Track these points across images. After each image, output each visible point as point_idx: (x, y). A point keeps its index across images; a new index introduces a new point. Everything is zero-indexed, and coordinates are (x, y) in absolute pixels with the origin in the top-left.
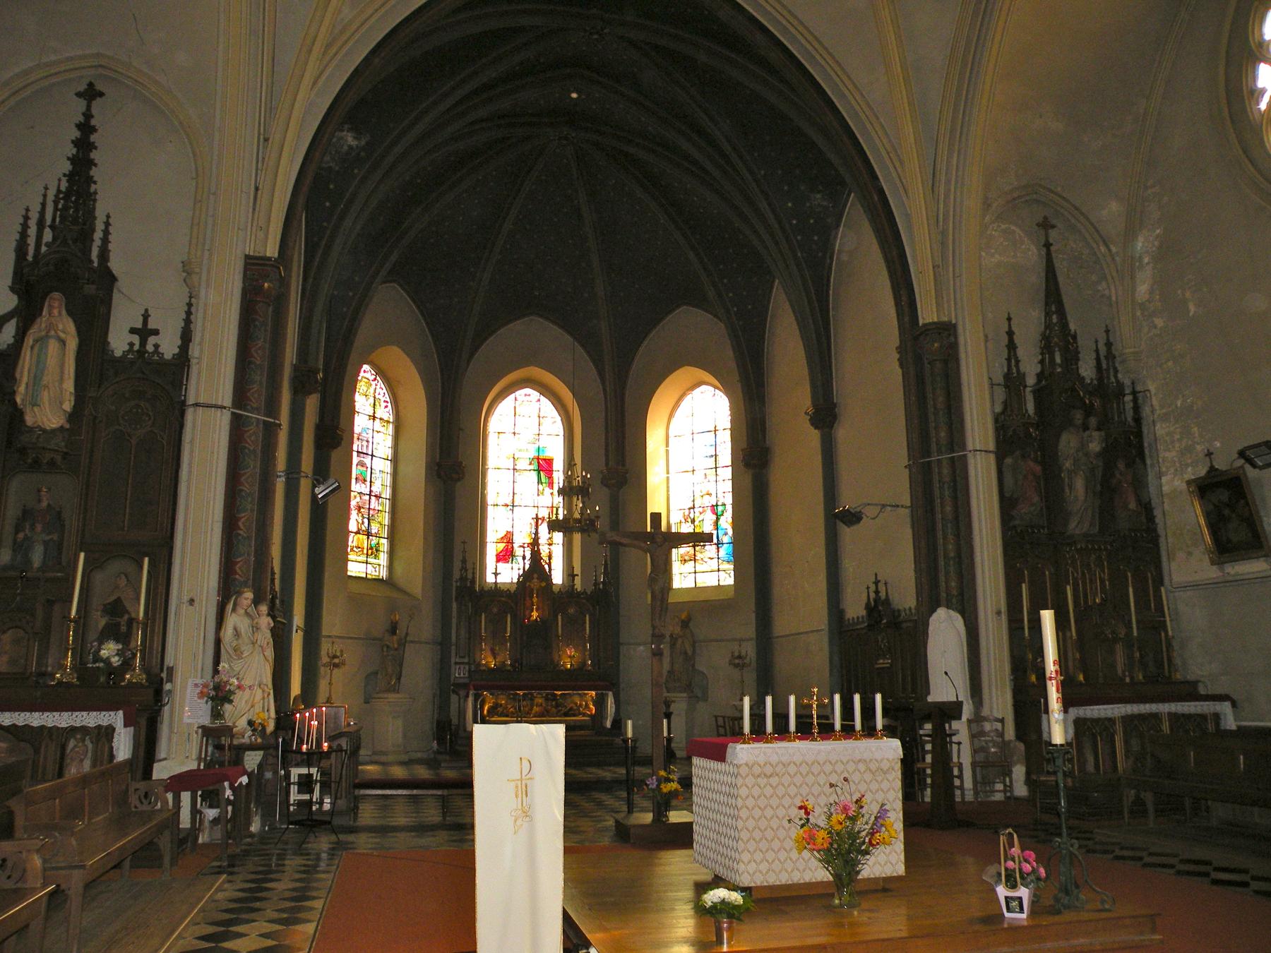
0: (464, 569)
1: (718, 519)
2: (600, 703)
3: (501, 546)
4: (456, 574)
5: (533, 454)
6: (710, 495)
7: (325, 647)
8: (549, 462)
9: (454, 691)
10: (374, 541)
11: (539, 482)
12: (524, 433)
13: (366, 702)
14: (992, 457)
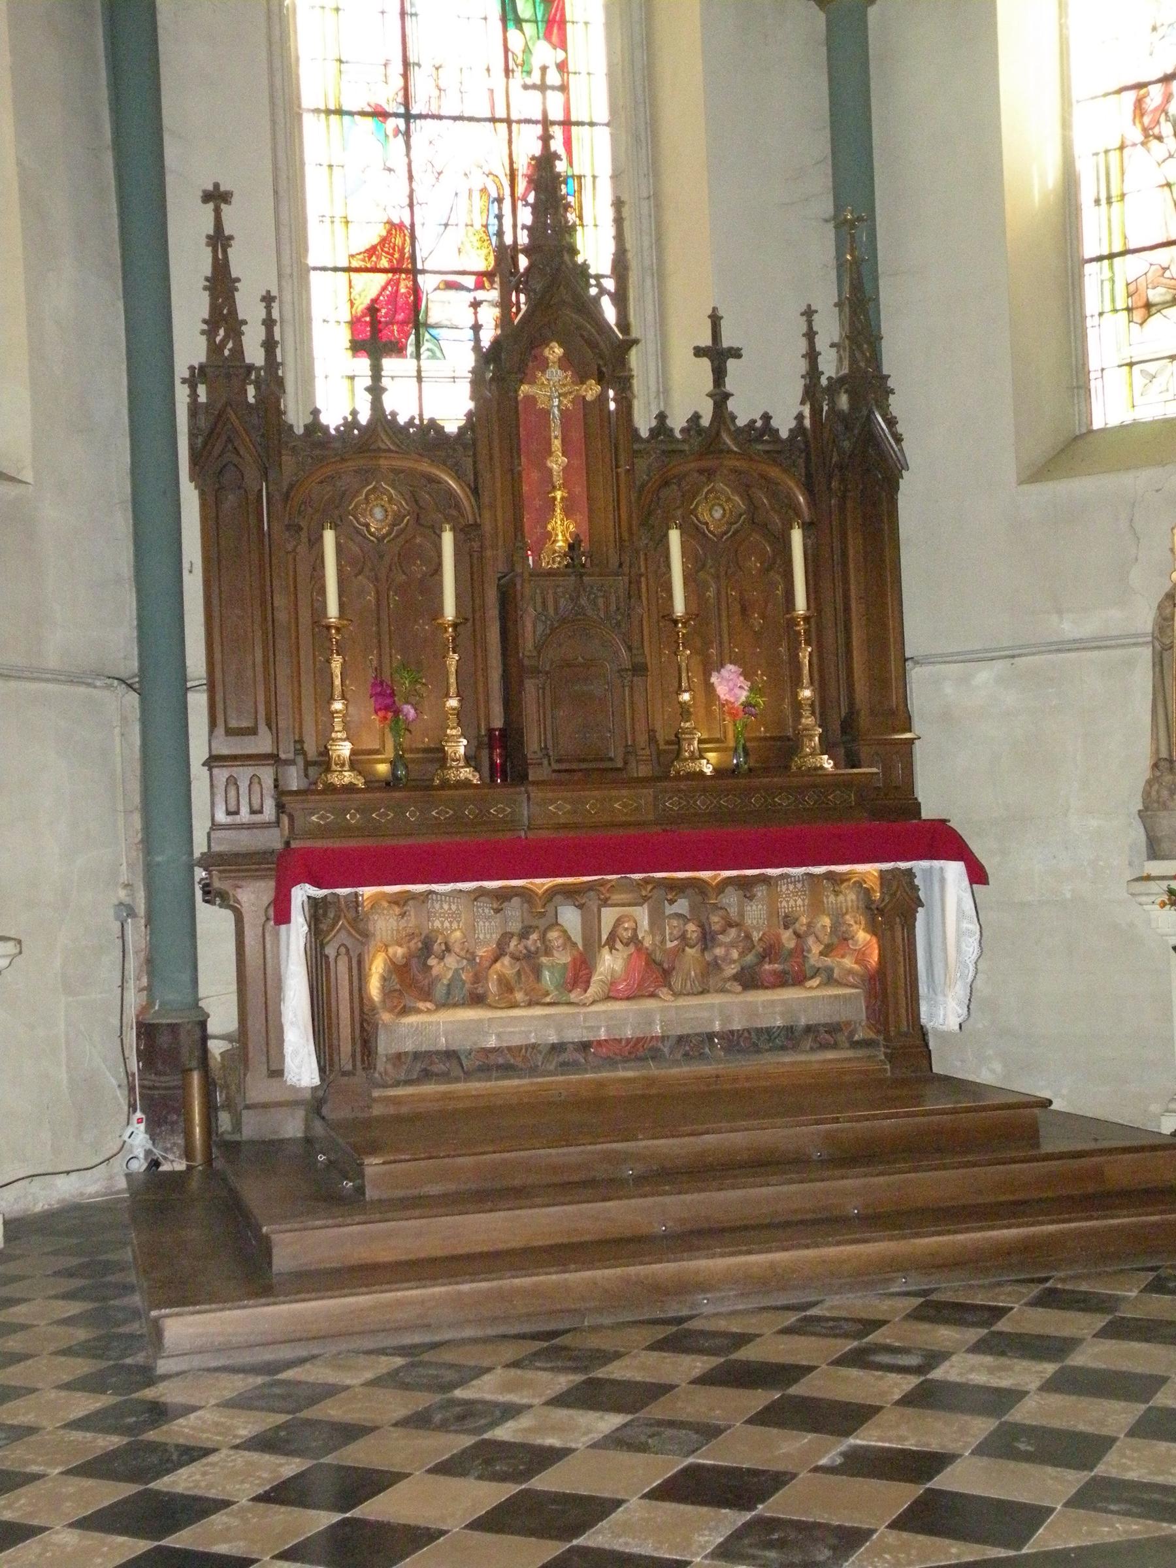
0: (223, 317)
3: (371, 286)
4: (190, 348)
9: (210, 894)
14: (568, 17)
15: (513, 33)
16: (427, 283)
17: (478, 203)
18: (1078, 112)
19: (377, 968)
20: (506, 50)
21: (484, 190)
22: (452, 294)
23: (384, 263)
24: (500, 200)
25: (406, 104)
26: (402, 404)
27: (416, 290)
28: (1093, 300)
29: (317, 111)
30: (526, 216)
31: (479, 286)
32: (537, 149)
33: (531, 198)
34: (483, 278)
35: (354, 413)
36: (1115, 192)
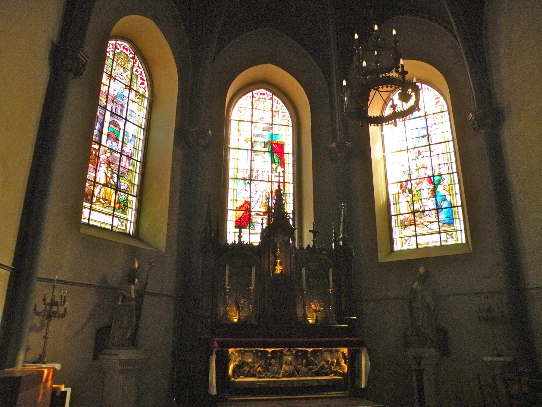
1: (435, 188)
2: (353, 360)
5: (267, 139)
6: (426, 168)
7: (39, 295)
8: (281, 146)
10: (123, 197)
11: (273, 161)
12: (259, 130)
13: (96, 358)
15: (274, 165)
16: (253, 214)
17: (264, 198)
18: (389, 186)
19: (231, 367)
20: (272, 168)
21: (266, 195)
22: (257, 216)
23: (244, 209)
24: (269, 198)
25: (251, 177)
26: (245, 239)
27: (250, 215)
28: (393, 224)
29: (232, 178)
30: (274, 201)
31: (264, 215)
32: (277, 188)
33: (275, 198)
34: (264, 213)
35: (235, 241)
36: (397, 202)
